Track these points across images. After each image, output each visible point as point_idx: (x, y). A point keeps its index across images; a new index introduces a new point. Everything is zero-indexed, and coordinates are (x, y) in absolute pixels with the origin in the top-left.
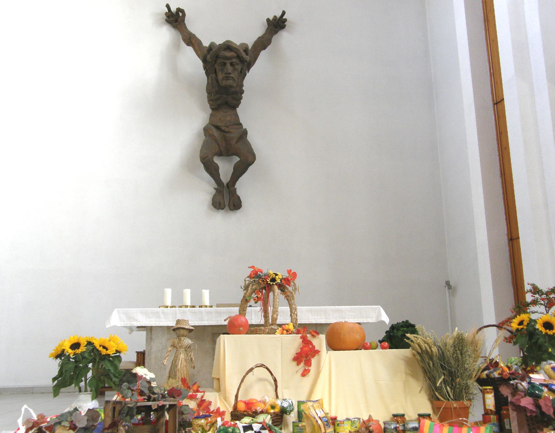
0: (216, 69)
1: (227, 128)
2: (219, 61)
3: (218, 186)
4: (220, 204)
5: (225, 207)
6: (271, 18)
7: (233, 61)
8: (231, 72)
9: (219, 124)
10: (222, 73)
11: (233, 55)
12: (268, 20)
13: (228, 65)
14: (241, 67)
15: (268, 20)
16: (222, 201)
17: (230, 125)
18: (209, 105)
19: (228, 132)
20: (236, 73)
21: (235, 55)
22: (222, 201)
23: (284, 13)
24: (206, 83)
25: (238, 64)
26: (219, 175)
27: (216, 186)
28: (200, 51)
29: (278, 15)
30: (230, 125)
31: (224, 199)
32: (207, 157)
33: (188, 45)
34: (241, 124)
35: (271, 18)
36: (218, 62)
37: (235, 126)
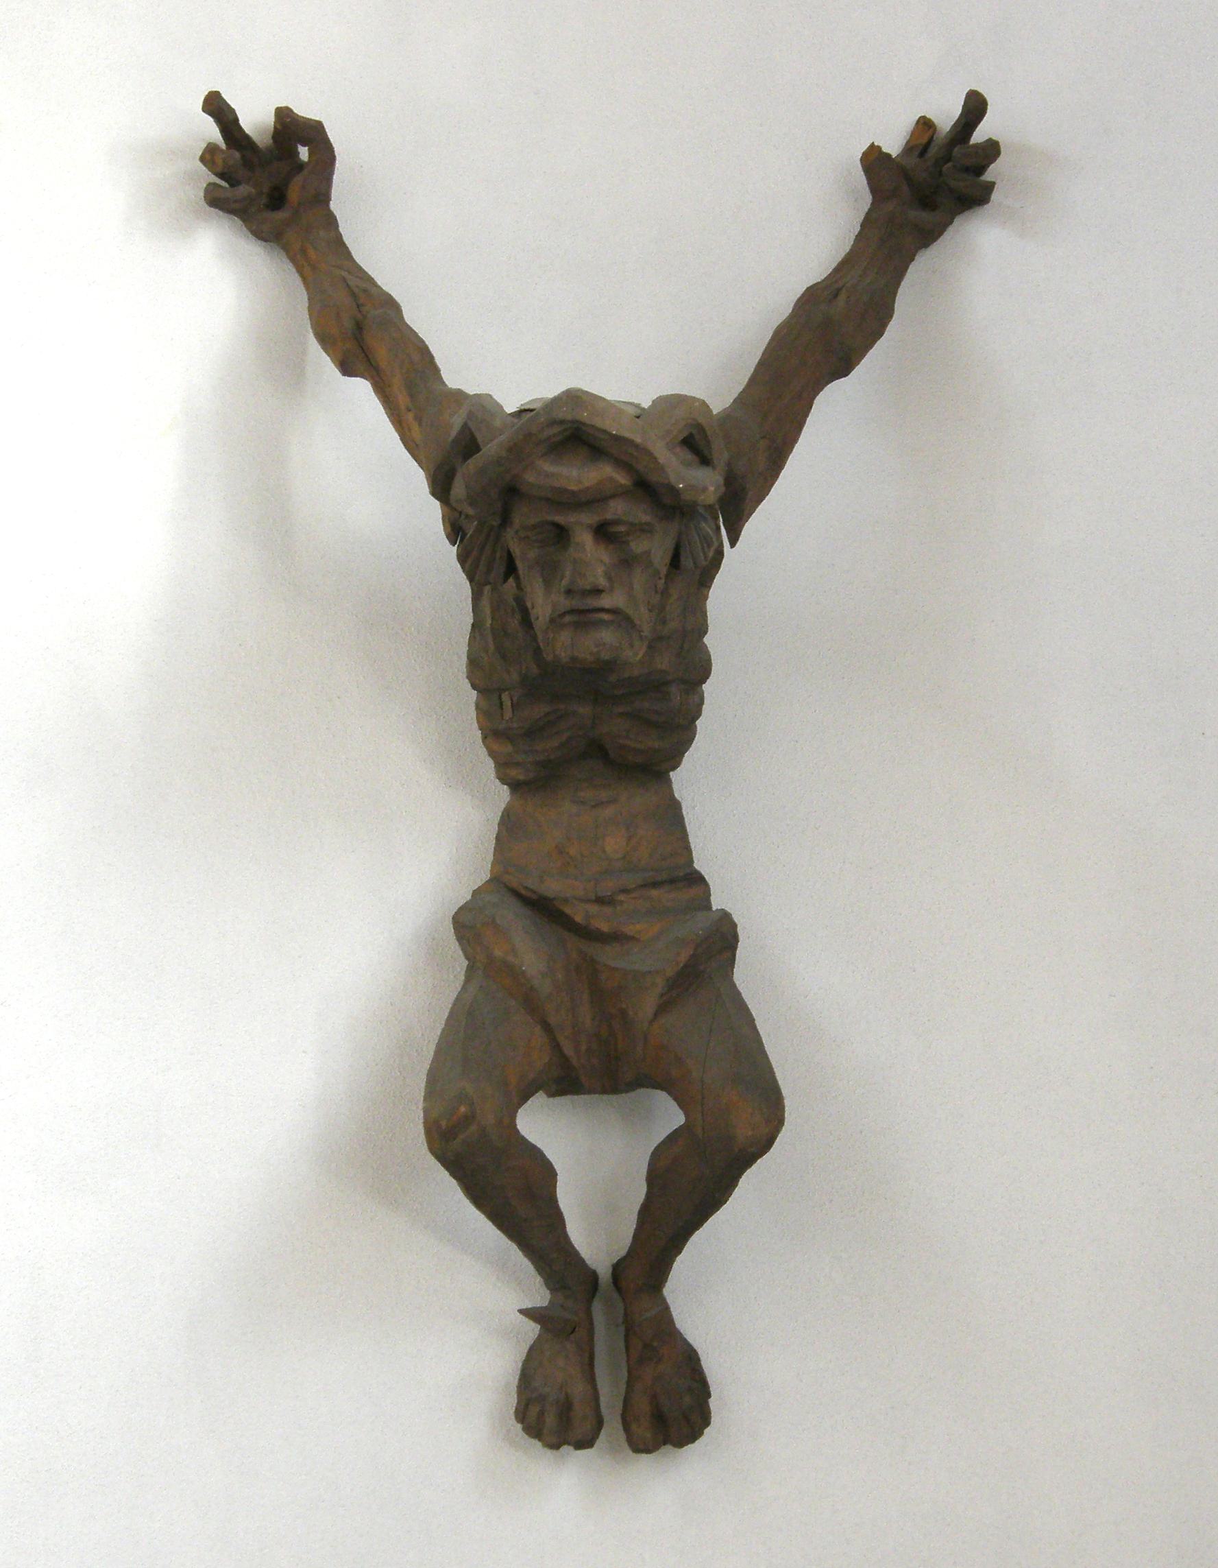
0: (509, 554)
1: (607, 910)
2: (523, 516)
3: (553, 1290)
4: (566, 1409)
5: (600, 1423)
6: (893, 145)
7: (609, 516)
8: (602, 582)
9: (552, 887)
10: (548, 584)
11: (611, 479)
12: (874, 160)
13: (585, 539)
14: (670, 543)
15: (874, 160)
16: (578, 1389)
17: (624, 891)
18: (490, 764)
19: (615, 937)
20: (639, 579)
21: (623, 479)
22: (578, 1389)
23: (975, 107)
24: (469, 619)
25: (644, 530)
26: (556, 1219)
27: (540, 1296)
28: (419, 419)
29: (947, 112)
30: (624, 891)
31: (591, 1379)
32: (469, 1119)
33: (347, 369)
34: (697, 880)
35: (893, 145)
36: (517, 520)
37: (654, 893)
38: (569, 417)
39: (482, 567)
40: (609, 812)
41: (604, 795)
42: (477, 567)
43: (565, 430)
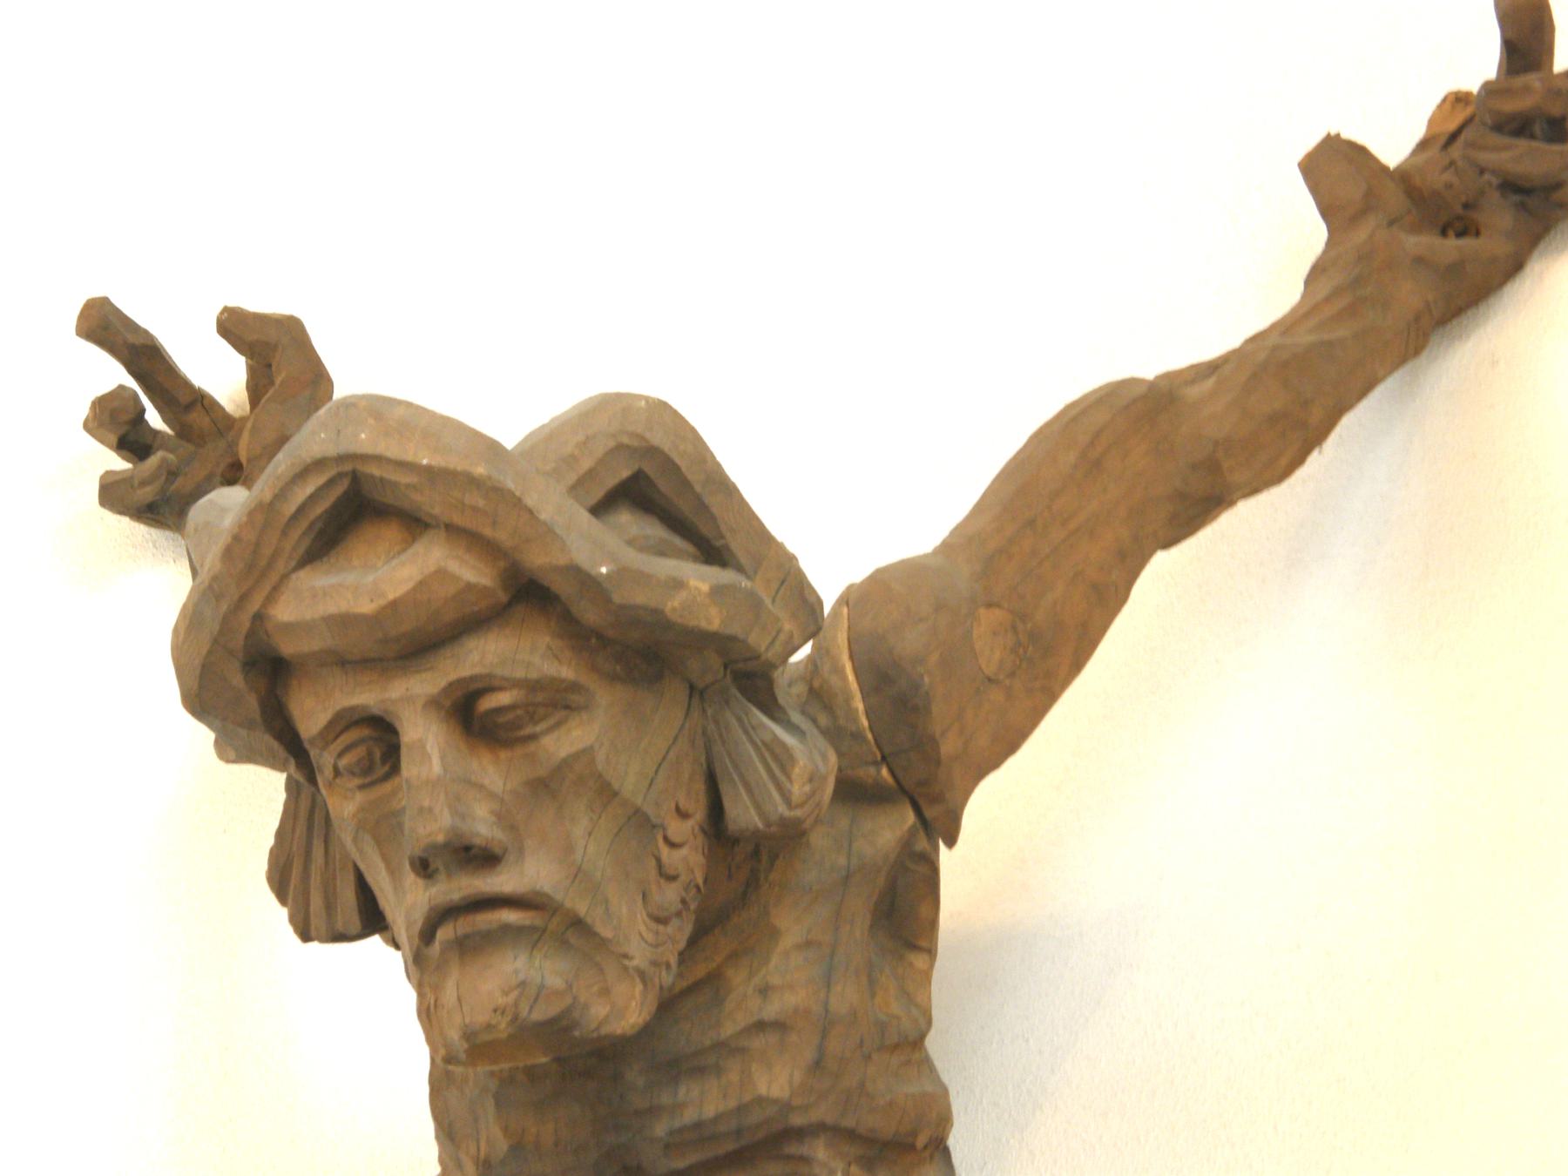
12: (1329, 135)
15: (1329, 135)
38: (331, 450)
42: (307, 904)
43: (330, 483)
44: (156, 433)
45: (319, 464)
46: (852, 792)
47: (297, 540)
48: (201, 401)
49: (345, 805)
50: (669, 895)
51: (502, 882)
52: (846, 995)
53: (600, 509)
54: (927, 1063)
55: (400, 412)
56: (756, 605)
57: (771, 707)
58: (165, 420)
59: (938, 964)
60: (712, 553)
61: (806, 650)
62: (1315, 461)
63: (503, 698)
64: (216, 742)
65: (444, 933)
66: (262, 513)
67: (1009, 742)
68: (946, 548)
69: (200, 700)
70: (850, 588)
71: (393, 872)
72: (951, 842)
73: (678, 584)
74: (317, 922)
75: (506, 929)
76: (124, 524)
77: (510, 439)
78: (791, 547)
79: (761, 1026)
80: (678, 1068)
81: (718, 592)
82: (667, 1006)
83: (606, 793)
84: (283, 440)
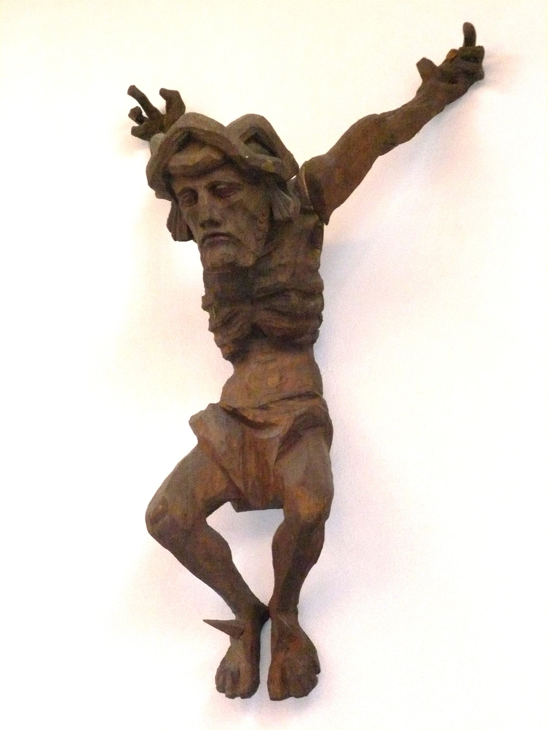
13: (204, 195)
21: (216, 156)
35: (438, 60)
39: (178, 232)
40: (272, 366)
41: (269, 357)
44: (145, 118)
45: (181, 129)
46: (304, 212)
47: (175, 148)
48: (155, 110)
49: (185, 211)
50: (260, 234)
51: (222, 230)
52: (301, 259)
53: (247, 142)
54: (318, 275)
55: (200, 117)
56: (282, 166)
57: (286, 191)
58: (147, 114)
59: (322, 252)
60: (273, 153)
61: (295, 177)
62: (417, 136)
63: (222, 187)
64: (156, 194)
65: (207, 241)
66: (167, 140)
67: (341, 201)
68: (329, 153)
69: (152, 184)
70: (306, 162)
71: (195, 225)
72: (327, 224)
73: (265, 161)
74: (178, 235)
75: (221, 240)
76: (137, 139)
77: (226, 123)
78: (292, 152)
79: (280, 265)
80: (261, 274)
81: (274, 164)
82: (259, 260)
83: (245, 210)
84: (174, 121)
